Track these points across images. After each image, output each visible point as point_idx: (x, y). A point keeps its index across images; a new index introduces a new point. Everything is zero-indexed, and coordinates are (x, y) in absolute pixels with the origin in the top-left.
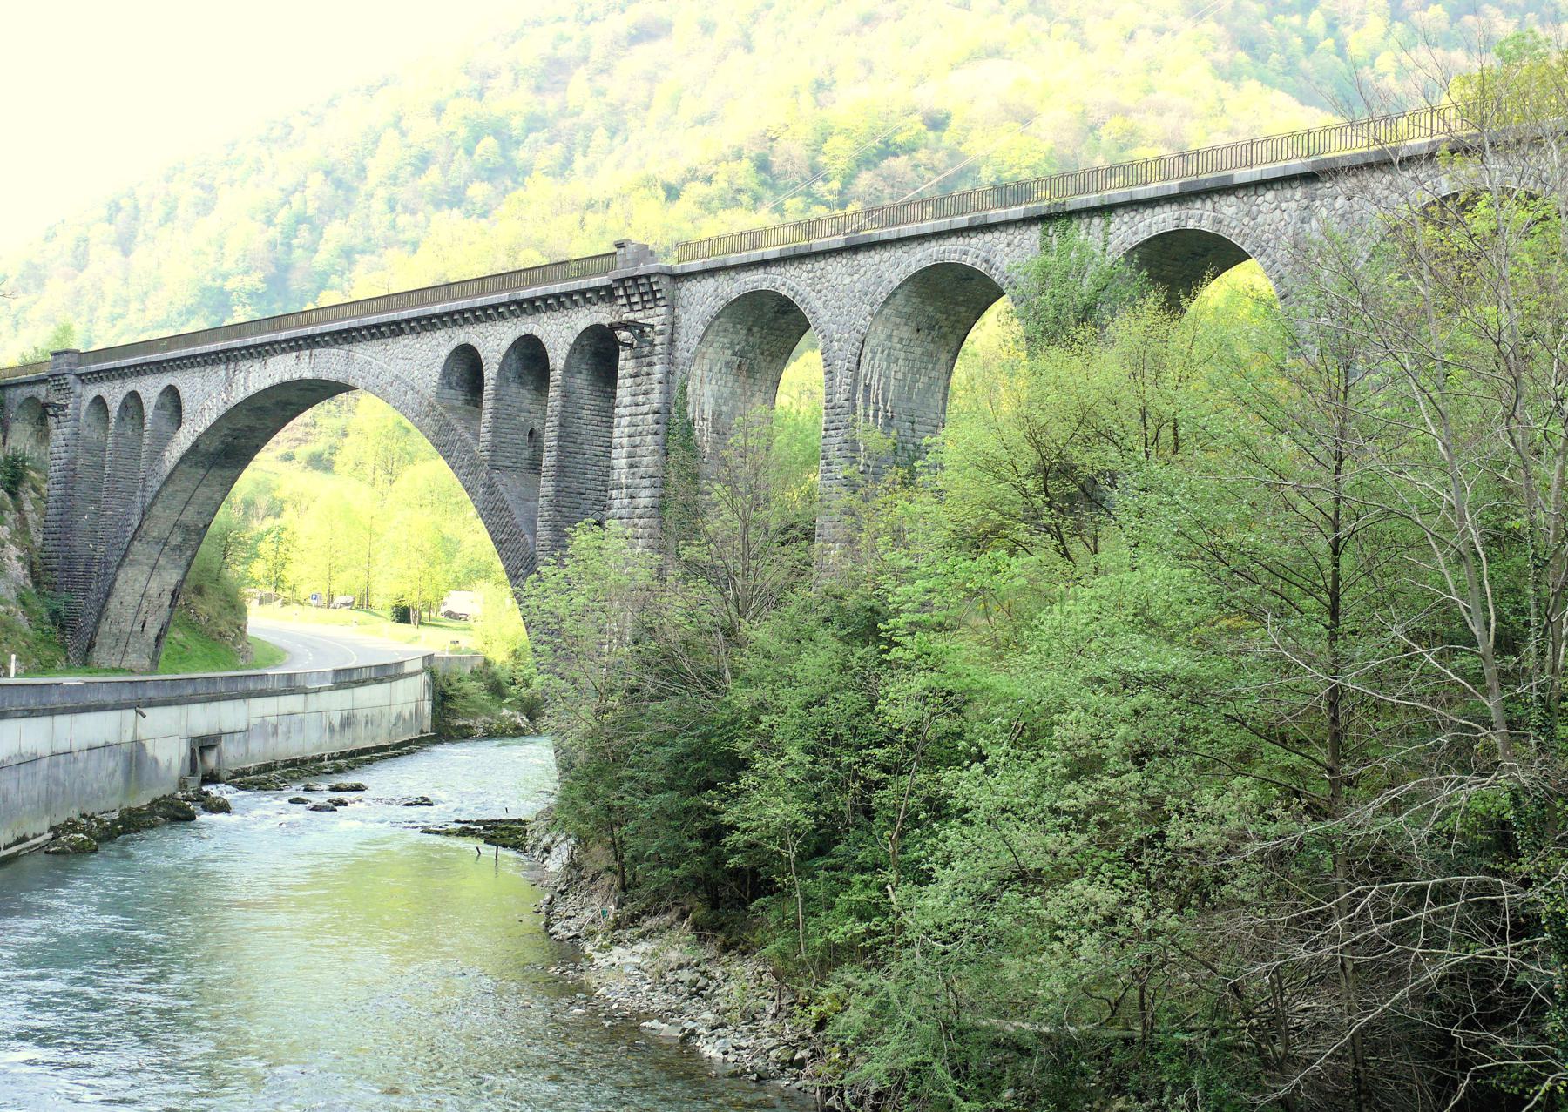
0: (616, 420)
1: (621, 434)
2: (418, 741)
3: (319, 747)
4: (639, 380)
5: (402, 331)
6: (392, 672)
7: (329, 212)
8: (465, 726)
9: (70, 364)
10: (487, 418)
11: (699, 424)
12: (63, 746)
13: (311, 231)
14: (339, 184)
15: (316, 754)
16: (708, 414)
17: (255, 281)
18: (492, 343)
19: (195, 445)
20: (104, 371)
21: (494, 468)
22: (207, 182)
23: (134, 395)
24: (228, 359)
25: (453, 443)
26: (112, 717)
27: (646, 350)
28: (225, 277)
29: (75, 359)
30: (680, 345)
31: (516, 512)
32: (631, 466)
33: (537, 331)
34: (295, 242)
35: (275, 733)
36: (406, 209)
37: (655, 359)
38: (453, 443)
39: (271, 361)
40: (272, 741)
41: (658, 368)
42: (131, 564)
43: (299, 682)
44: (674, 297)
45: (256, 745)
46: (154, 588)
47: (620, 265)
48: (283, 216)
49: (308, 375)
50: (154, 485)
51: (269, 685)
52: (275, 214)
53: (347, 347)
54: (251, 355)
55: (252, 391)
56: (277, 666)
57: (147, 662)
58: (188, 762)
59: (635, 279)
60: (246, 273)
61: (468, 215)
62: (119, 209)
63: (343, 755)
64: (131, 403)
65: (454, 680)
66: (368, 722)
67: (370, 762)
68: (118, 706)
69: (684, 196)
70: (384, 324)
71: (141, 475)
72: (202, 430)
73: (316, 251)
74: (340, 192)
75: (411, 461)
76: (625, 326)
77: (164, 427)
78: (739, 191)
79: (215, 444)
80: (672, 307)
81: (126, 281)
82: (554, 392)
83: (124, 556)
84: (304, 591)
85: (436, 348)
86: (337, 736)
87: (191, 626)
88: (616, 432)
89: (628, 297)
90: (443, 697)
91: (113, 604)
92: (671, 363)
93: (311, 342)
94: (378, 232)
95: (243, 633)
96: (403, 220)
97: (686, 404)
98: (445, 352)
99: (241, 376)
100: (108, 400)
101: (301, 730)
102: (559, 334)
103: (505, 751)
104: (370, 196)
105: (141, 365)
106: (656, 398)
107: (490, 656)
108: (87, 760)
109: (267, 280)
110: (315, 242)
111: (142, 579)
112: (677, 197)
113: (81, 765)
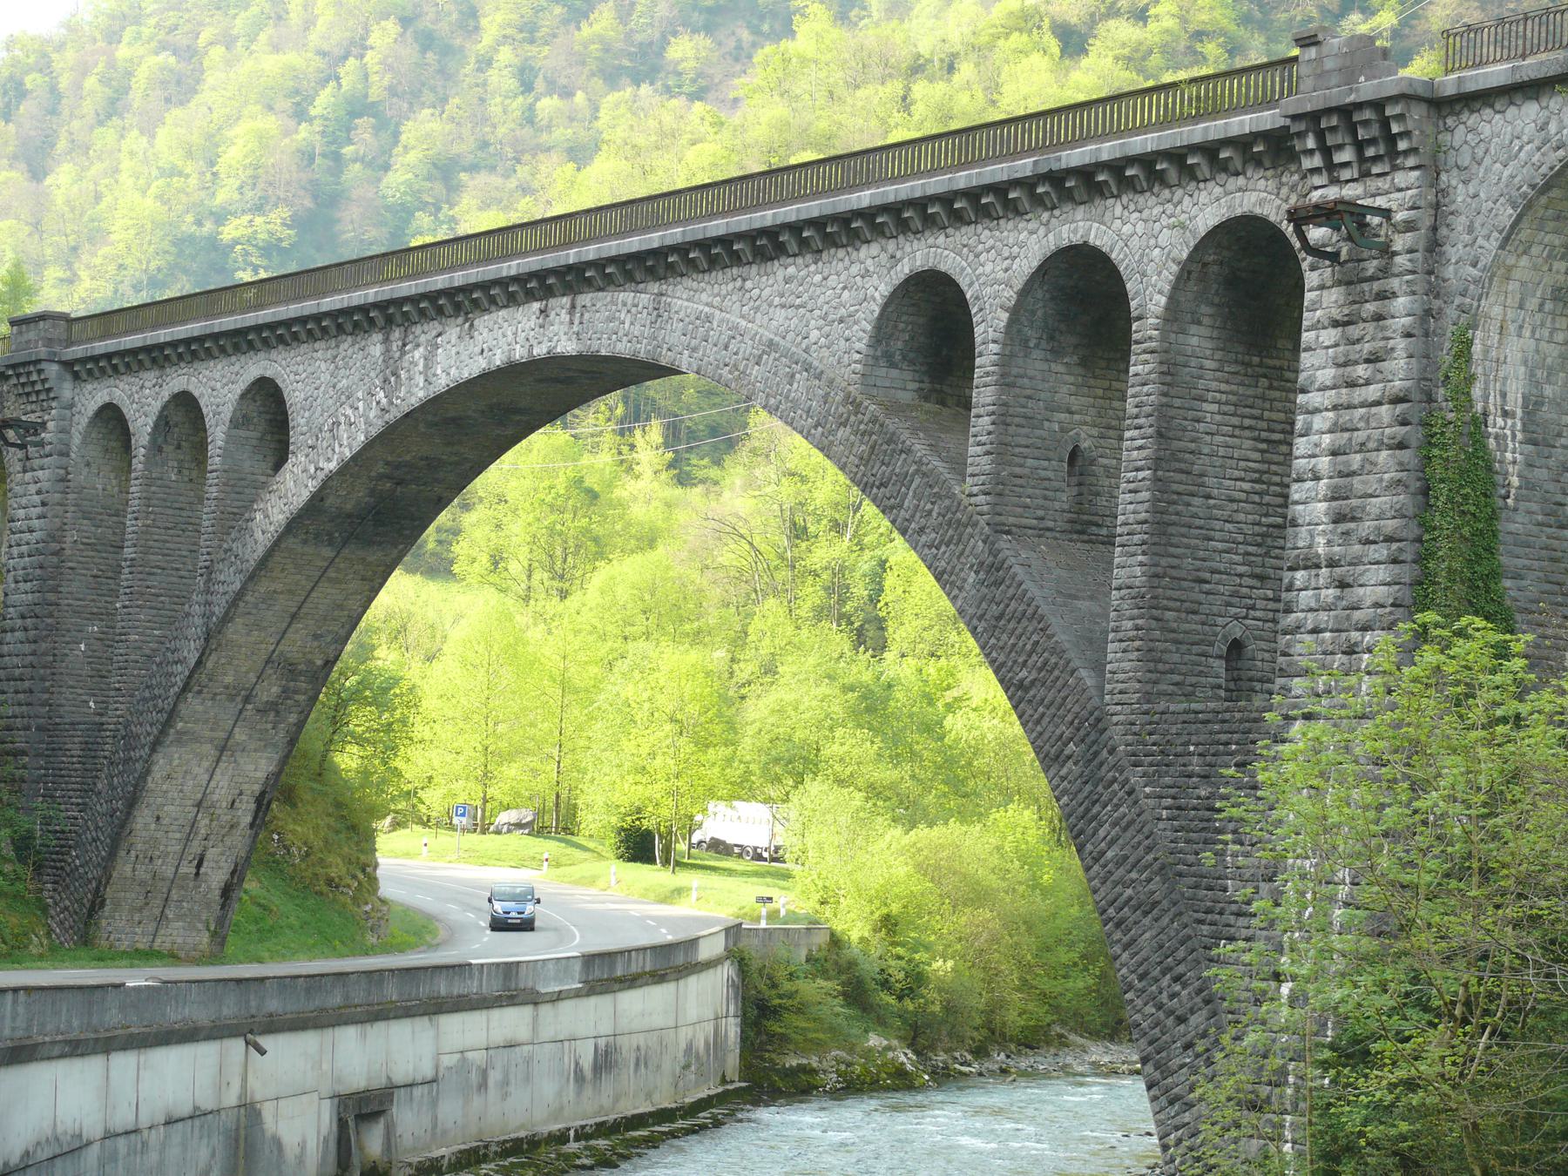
0: (1300, 421)
1: (1313, 446)
2: (721, 1099)
3: (557, 1114)
4: (1354, 331)
5: (780, 251)
6: (680, 959)
7: (410, 94)
8: (802, 1069)
9: (49, 342)
10: (982, 423)
11: (1496, 424)
12: (123, 1118)
13: (377, 130)
14: (427, 41)
15: (555, 1127)
16: (1515, 403)
17: (273, 223)
18: (990, 267)
19: (317, 499)
20: (121, 354)
21: (1000, 529)
22: (180, 39)
23: (185, 402)
24: (390, 321)
25: (905, 480)
26: (205, 1054)
27: (1371, 267)
28: (220, 217)
29: (59, 331)
30: (1453, 252)
31: (1056, 623)
32: (1339, 518)
33: (1099, 236)
34: (348, 150)
35: (483, 1085)
36: (552, 88)
37: (1395, 283)
38: (905, 480)
39: (483, 322)
40: (477, 1102)
41: (1401, 303)
42: (179, 741)
43: (525, 980)
44: (1438, 148)
45: (451, 1111)
46: (222, 790)
47: (1307, 84)
48: (324, 101)
49: (567, 347)
50: (230, 579)
51: (472, 987)
52: (310, 100)
53: (654, 287)
54: (440, 311)
55: (442, 382)
56: (435, 947)
57: (205, 939)
58: (333, 1146)
59: (1346, 112)
60: (259, 209)
61: (668, 91)
62: (21, 93)
63: (602, 1129)
64: (177, 417)
65: (781, 974)
66: (641, 1061)
67: (652, 1142)
68: (216, 1032)
69: (1096, 47)
70: (740, 236)
71: (202, 561)
72: (333, 466)
73: (386, 168)
74: (430, 56)
75: (600, 555)
76: (1327, 214)
77: (251, 464)
78: (1199, 35)
79: (356, 496)
80: (1433, 169)
81: (37, 226)
82: (1140, 366)
83: (163, 732)
84: (434, 801)
85: (864, 281)
86: (588, 1091)
87: (274, 866)
88: (1301, 445)
89: (1327, 152)
90: (761, 1009)
91: (142, 820)
92: (1434, 291)
93: (573, 279)
94: (502, 130)
95: (373, 880)
96: (548, 105)
97: (1470, 380)
98: (881, 289)
99: (418, 354)
100: (129, 411)
101: (528, 1078)
102: (1152, 243)
103: (902, 1123)
104: (486, 63)
105: (200, 339)
106: (1399, 369)
107: (838, 927)
108: (163, 1146)
109: (295, 222)
110: (387, 152)
111: (200, 771)
112: (1082, 50)
113: (153, 1156)
